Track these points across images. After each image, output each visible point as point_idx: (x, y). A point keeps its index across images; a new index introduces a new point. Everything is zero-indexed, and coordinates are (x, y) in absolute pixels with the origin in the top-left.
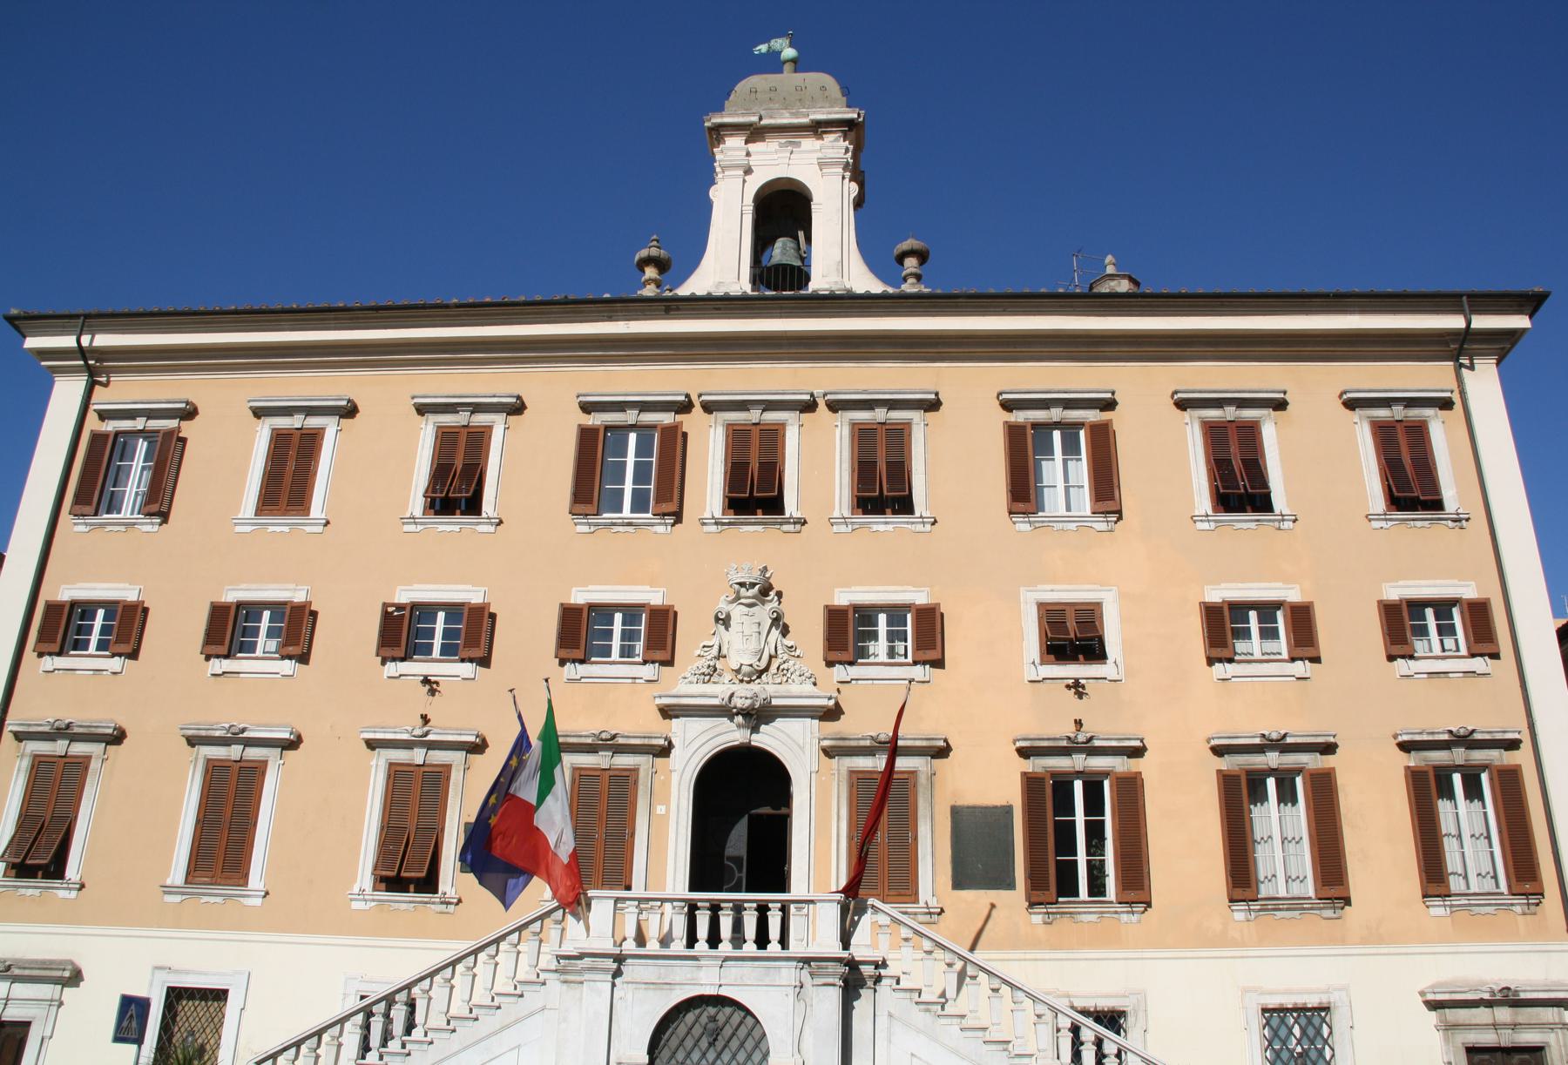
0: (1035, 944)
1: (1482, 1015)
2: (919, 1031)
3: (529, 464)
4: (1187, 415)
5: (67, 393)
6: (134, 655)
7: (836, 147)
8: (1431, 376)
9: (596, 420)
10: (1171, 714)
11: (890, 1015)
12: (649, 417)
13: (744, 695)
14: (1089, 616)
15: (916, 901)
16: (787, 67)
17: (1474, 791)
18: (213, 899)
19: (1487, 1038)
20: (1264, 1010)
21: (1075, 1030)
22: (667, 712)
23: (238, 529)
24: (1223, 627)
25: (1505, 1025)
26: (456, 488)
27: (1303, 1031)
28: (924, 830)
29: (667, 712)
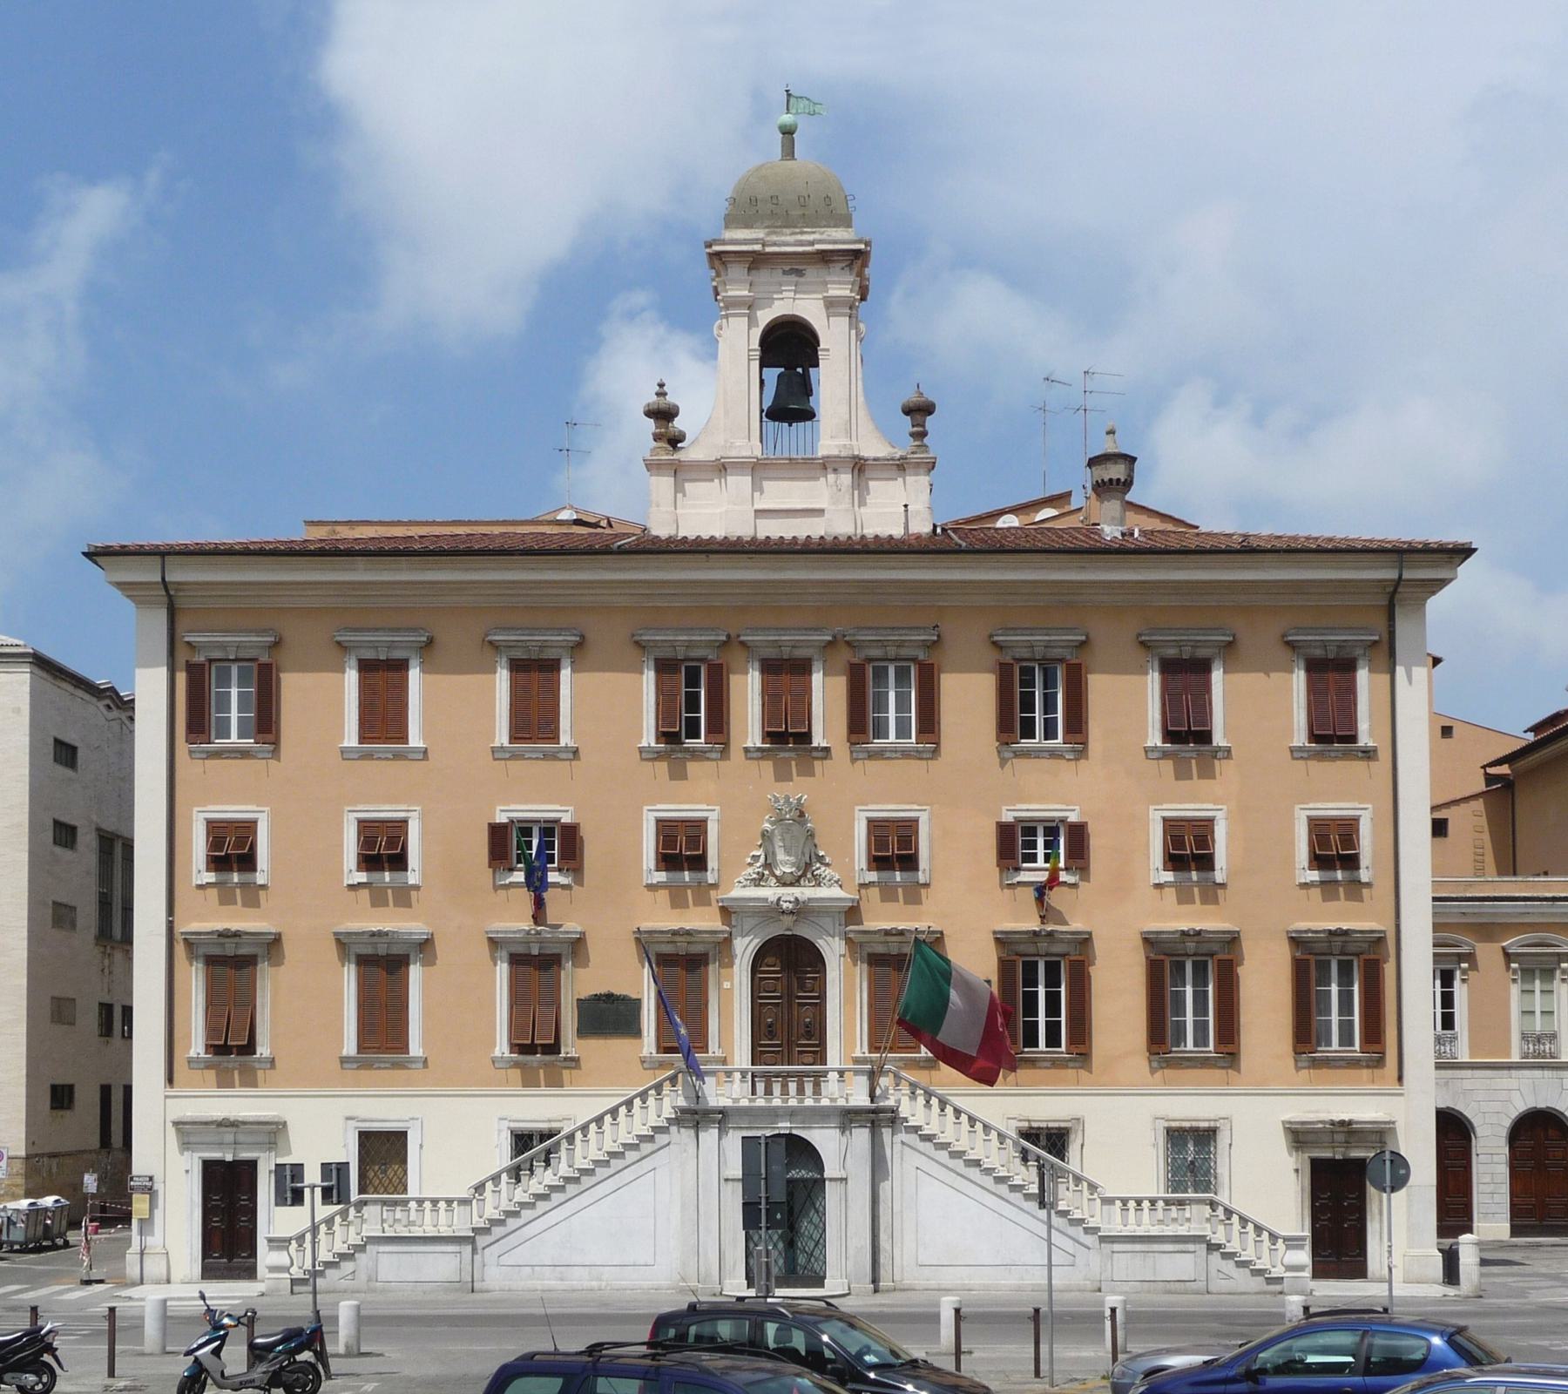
10: (1268, 905)
19: (1327, 1154)
20: (1170, 1132)
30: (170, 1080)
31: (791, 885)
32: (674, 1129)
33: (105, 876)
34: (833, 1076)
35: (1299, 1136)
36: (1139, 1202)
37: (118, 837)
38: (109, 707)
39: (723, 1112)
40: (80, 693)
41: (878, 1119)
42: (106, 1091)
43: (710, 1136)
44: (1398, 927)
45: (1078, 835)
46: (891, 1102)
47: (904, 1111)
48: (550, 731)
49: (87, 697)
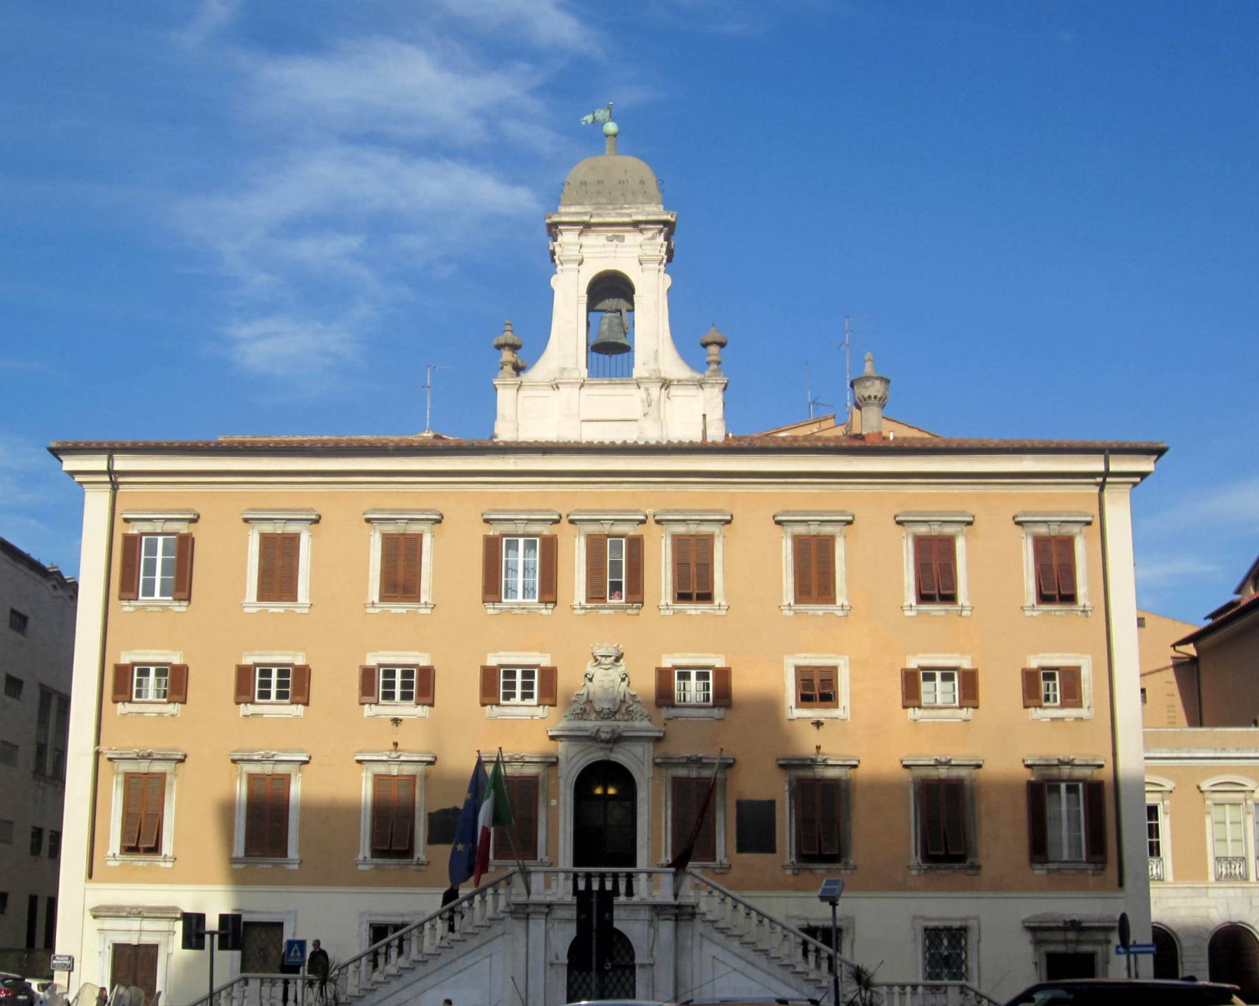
0: (785, 886)
1: (1059, 936)
2: (718, 944)
3: (447, 564)
5: (96, 503)
6: (184, 702)
7: (655, 245)
9: (493, 531)
11: (701, 935)
12: (534, 528)
13: (606, 726)
15: (714, 860)
16: (609, 143)
19: (1061, 949)
21: (805, 943)
23: (246, 610)
25: (1071, 942)
26: (401, 579)
27: (949, 942)
28: (719, 816)
30: (90, 875)
31: (608, 718)
32: (509, 921)
33: (43, 721)
34: (643, 877)
35: (1037, 931)
36: (903, 987)
37: (56, 692)
38: (54, 587)
39: (549, 906)
40: (32, 574)
41: (682, 914)
42: (33, 900)
43: (538, 927)
44: (1115, 754)
45: (427, 675)
46: (692, 901)
47: (703, 908)
49: (38, 577)
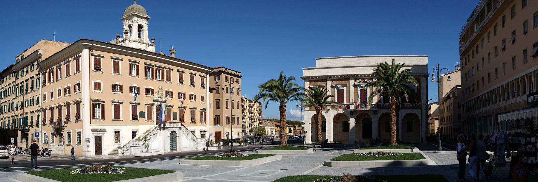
4: (112, 60)
8: (204, 75)
10: (107, 96)
14: (100, 84)
17: (99, 108)
18: (117, 121)
22: (154, 101)
24: (114, 87)
29: (154, 101)
48: (170, 80)
